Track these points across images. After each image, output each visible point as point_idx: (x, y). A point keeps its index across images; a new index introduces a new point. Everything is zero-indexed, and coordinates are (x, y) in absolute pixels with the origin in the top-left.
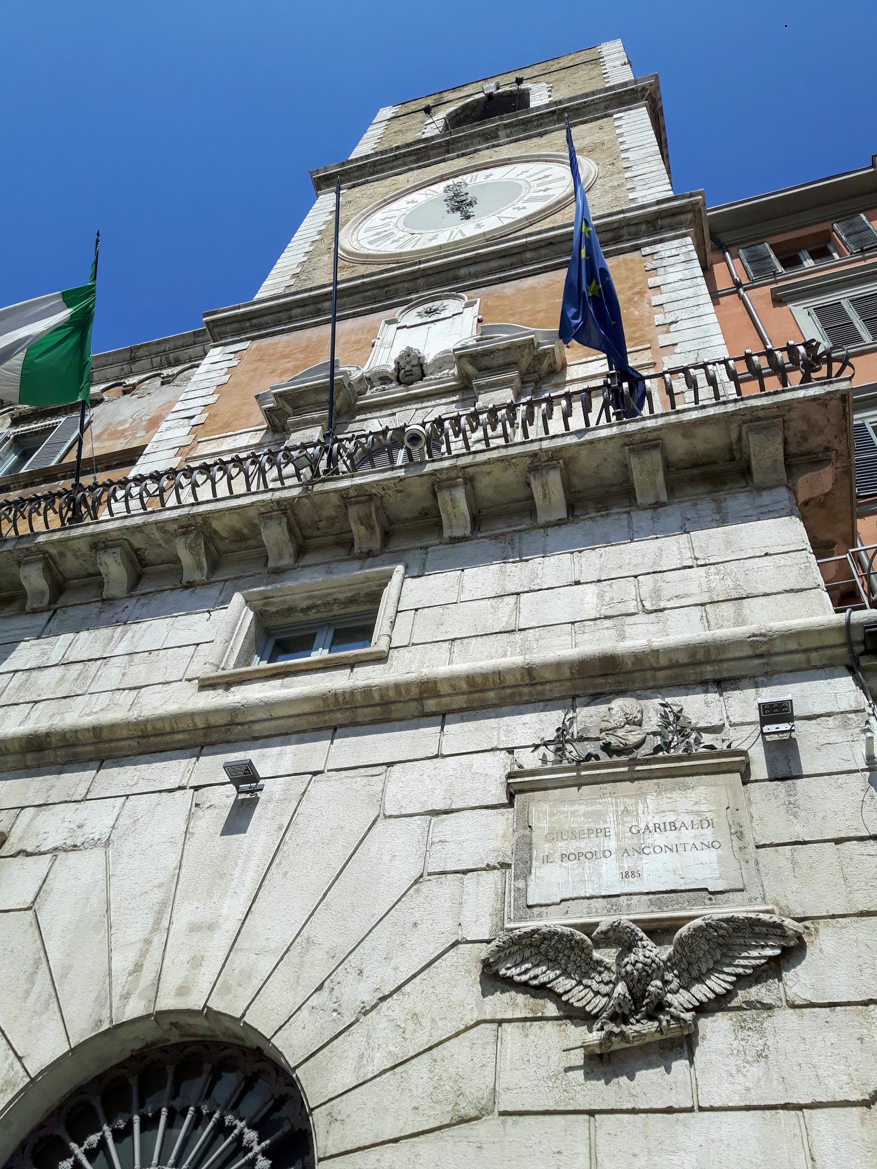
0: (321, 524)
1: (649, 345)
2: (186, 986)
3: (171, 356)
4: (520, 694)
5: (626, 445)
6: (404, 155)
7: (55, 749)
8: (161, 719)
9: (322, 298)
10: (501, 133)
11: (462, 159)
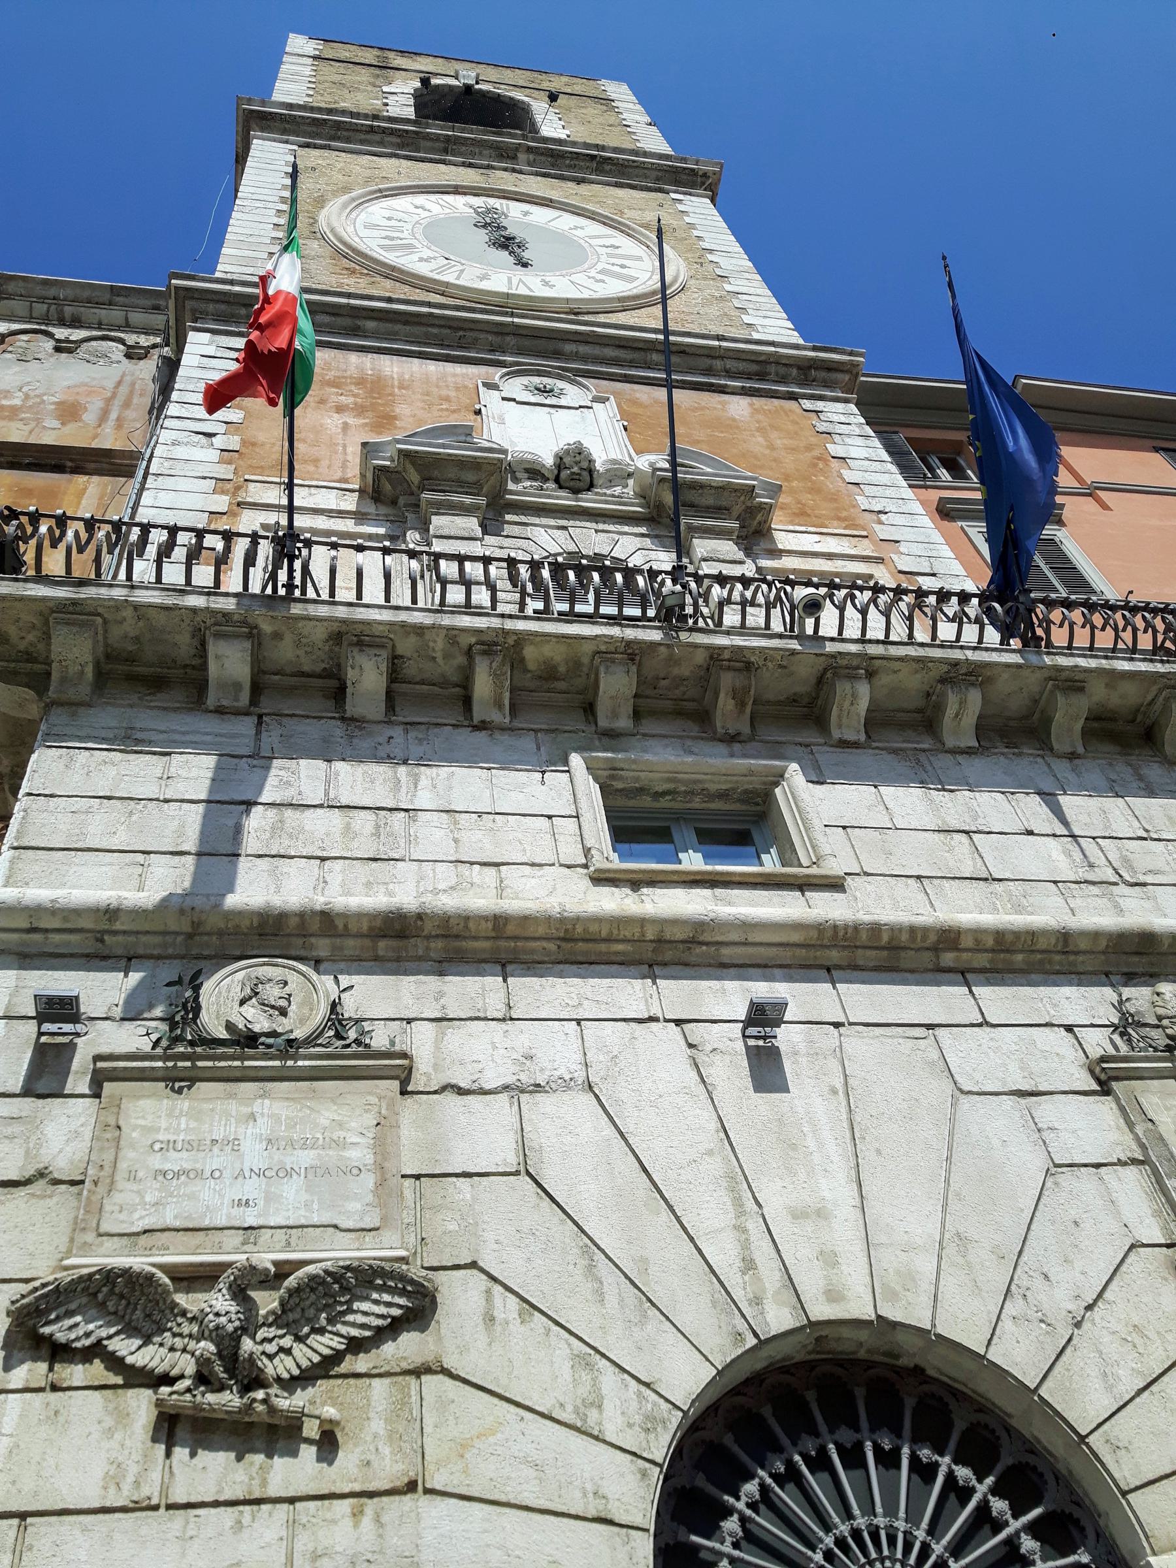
0: (663, 683)
1: (864, 533)
2: (846, 1293)
3: (68, 310)
4: (1050, 962)
5: (1050, 679)
6: (384, 131)
7: (428, 937)
8: (598, 920)
9: (364, 313)
10: (522, 156)
11: (469, 170)
